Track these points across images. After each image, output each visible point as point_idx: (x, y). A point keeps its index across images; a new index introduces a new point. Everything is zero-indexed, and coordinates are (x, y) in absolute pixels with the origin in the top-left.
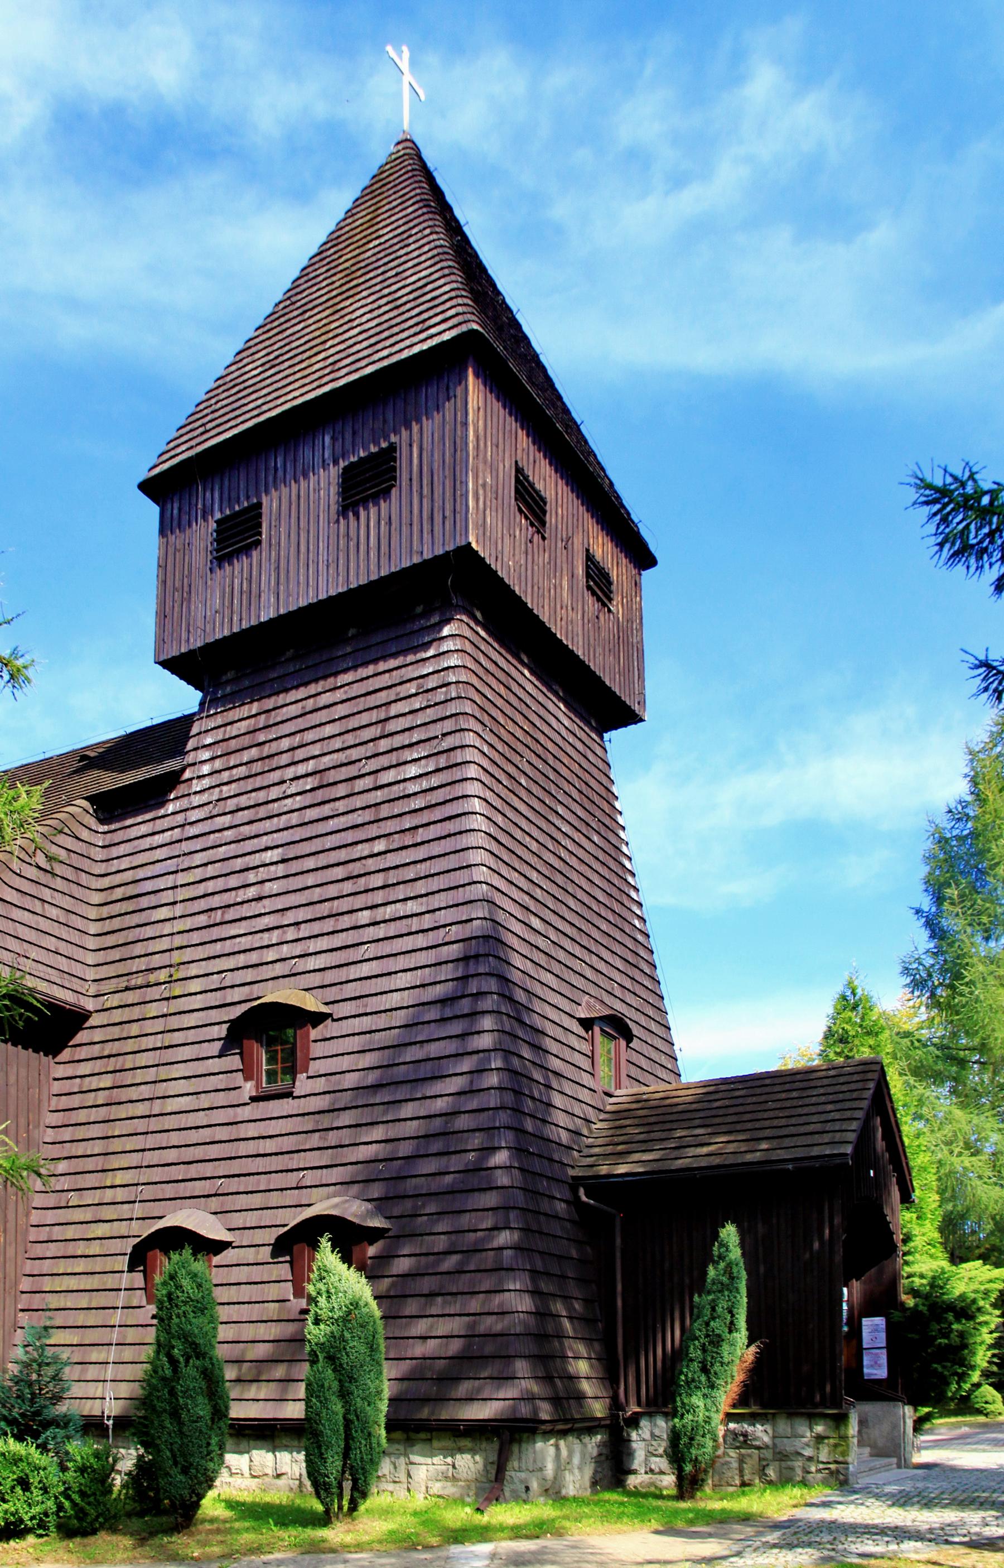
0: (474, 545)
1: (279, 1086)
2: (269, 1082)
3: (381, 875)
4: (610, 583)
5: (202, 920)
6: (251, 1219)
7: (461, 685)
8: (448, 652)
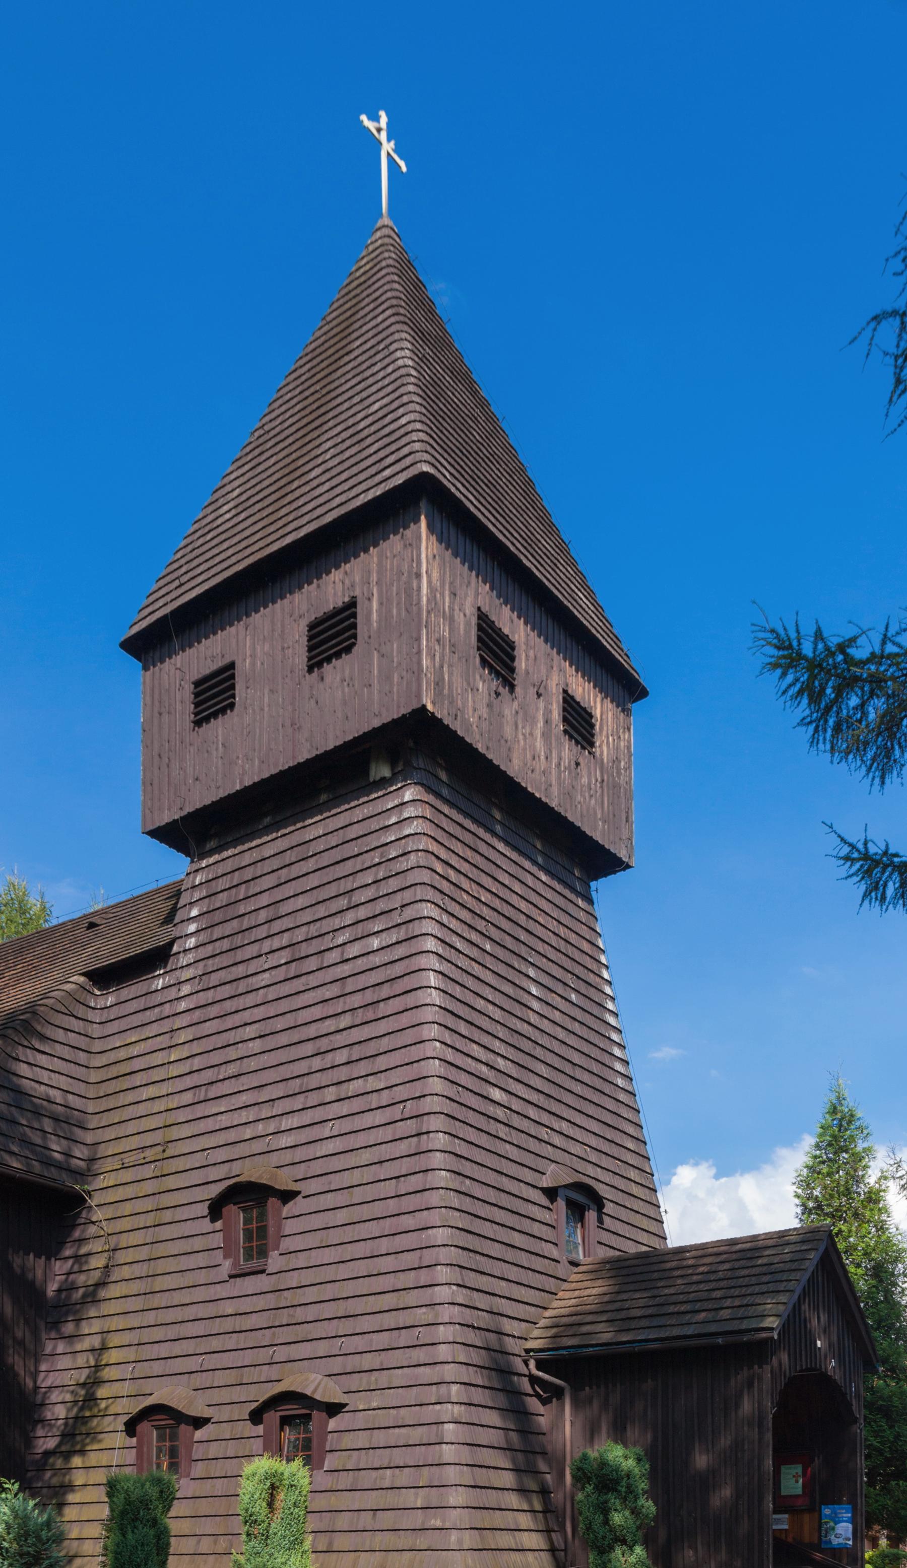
0: (430, 707)
1: (254, 1264)
2: (246, 1260)
3: (345, 1051)
4: (592, 726)
5: (188, 1098)
7: (420, 853)
8: (408, 818)
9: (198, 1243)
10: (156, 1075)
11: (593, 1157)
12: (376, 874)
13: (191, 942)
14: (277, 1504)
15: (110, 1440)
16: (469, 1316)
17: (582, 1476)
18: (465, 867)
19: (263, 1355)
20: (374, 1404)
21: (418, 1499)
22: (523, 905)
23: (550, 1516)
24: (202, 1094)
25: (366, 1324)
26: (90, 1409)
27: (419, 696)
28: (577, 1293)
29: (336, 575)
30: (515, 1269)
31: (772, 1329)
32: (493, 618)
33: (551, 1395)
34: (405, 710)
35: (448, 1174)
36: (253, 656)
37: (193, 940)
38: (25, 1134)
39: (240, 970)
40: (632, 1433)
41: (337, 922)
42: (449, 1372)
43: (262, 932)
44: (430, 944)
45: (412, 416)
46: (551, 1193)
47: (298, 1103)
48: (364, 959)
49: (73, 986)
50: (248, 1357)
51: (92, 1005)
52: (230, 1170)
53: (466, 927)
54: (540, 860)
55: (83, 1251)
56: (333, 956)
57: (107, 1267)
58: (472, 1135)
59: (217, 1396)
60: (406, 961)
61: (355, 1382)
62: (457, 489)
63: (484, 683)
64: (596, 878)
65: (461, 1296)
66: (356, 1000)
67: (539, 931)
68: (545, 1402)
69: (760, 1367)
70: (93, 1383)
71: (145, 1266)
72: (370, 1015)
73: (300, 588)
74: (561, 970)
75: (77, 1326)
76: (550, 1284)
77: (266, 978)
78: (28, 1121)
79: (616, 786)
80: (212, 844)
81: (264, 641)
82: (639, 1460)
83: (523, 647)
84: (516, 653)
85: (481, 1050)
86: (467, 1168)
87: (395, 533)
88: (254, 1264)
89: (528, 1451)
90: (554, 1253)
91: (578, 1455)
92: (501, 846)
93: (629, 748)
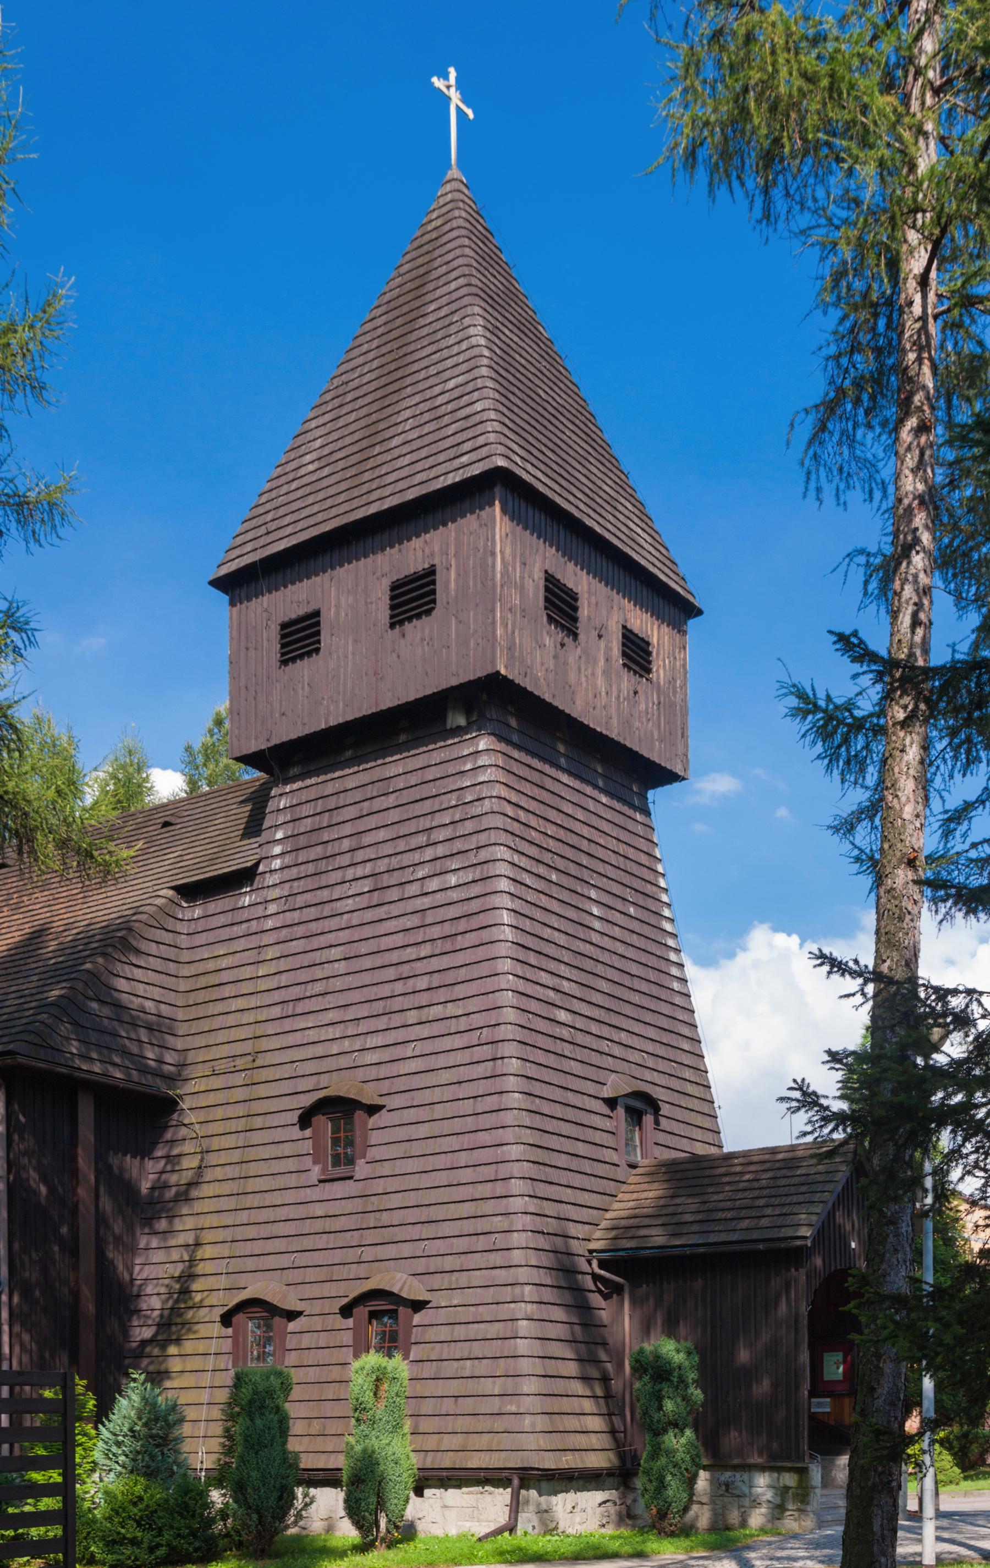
0: (503, 672)
2: (333, 1166)
3: (426, 978)
4: (649, 654)
5: (276, 1012)
6: (316, 1291)
9: (288, 1149)
10: (246, 988)
11: (650, 1062)
12: (453, 815)
13: (277, 864)
14: (380, 1393)
15: (203, 1330)
16: (539, 1223)
17: (640, 1367)
18: (533, 806)
19: (352, 1255)
20: (455, 1302)
21: (496, 1387)
22: (585, 831)
23: (611, 1404)
24: (289, 1009)
25: (448, 1229)
26: (185, 1302)
27: (493, 662)
28: (635, 1196)
29: (416, 543)
30: (580, 1176)
31: (806, 1238)
32: (558, 576)
33: (611, 1291)
34: (480, 674)
35: (520, 1096)
36: (338, 607)
37: (278, 861)
38: (125, 1046)
39: (325, 895)
40: (682, 1330)
41: (416, 857)
42: (523, 1274)
43: (345, 860)
44: (504, 885)
45: (485, 404)
46: (611, 1103)
47: (382, 1023)
48: (443, 893)
49: (164, 900)
50: (338, 1256)
51: (180, 916)
52: (318, 1082)
53: (534, 863)
54: (601, 783)
55: (175, 1152)
56: (413, 889)
57: (200, 1167)
58: (541, 1057)
59: (309, 1291)
60: (482, 899)
61: (436, 1282)
62: (528, 473)
63: (550, 637)
64: (654, 786)
65: (532, 1206)
66: (435, 932)
67: (600, 853)
68: (606, 1297)
69: (797, 1270)
70: (188, 1276)
71: (237, 1167)
72: (448, 946)
73: (383, 549)
74: (620, 886)
75: (171, 1223)
76: (610, 1187)
77: (350, 904)
78: (127, 1032)
79: (672, 705)
80: (295, 771)
81: (350, 594)
82: (689, 1353)
83: (586, 595)
84: (579, 604)
85: (548, 976)
86: (537, 1088)
87: (472, 513)
88: (341, 1171)
89: (590, 1343)
90: (615, 1158)
91: (637, 1348)
92: (565, 778)
93: (684, 666)
